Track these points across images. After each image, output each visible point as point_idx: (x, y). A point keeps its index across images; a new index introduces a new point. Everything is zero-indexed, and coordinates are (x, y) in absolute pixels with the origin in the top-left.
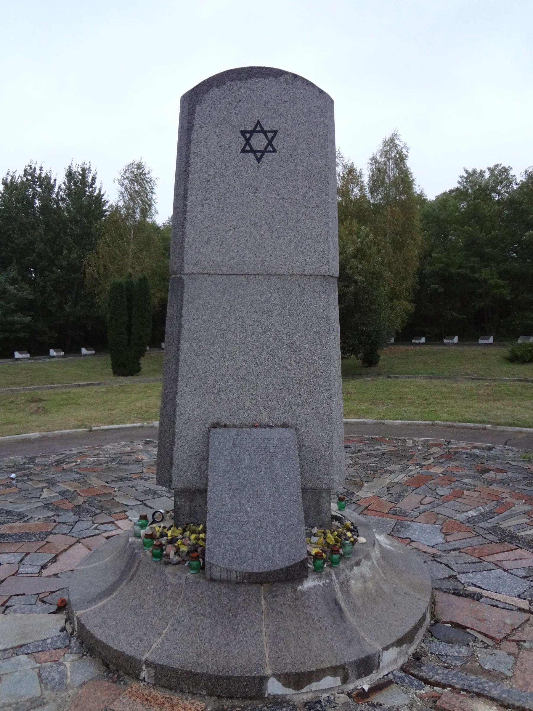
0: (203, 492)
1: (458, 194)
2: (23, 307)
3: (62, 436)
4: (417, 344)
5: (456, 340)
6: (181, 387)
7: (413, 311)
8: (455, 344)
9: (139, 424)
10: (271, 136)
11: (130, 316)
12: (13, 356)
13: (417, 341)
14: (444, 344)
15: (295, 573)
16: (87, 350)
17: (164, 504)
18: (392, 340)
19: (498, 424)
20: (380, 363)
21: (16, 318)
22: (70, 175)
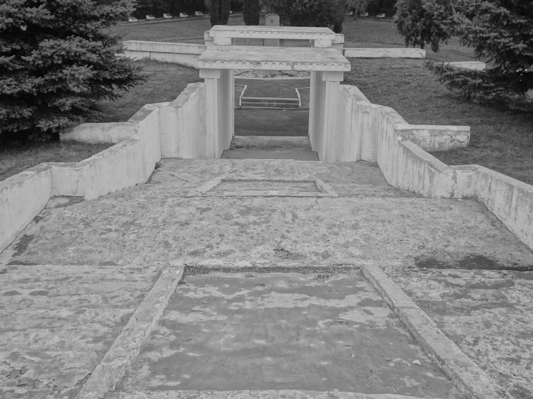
4: (379, 18)
13: (380, 16)
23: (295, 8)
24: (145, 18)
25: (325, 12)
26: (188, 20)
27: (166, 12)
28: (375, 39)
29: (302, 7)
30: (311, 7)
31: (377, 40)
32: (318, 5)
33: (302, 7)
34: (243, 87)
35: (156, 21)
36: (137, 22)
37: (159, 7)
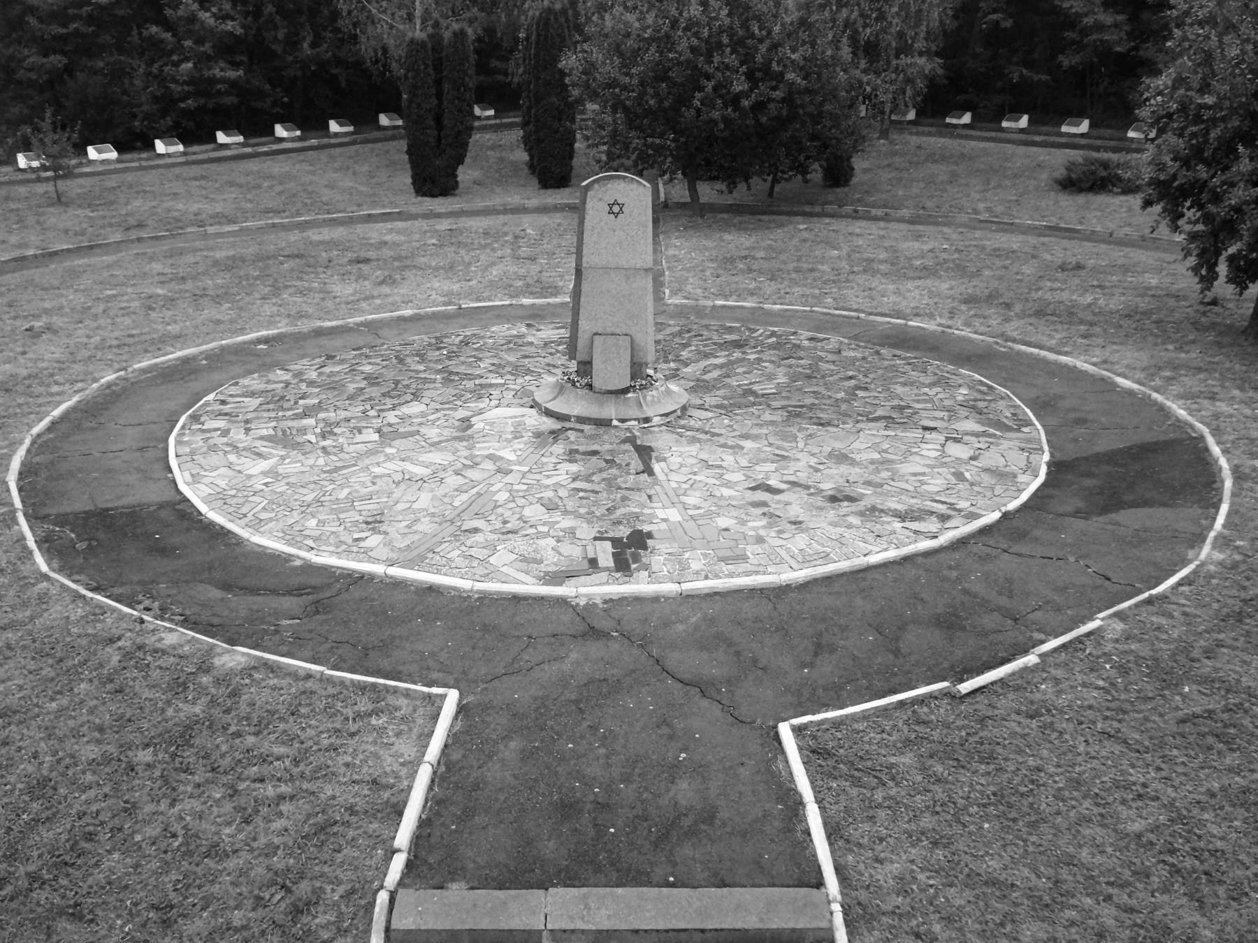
0: (590, 363)
2: (228, 48)
3: (434, 314)
4: (955, 126)
6: (581, 317)
9: (507, 303)
10: (621, 206)
11: (439, 95)
12: (272, 132)
13: (954, 121)
15: (625, 391)
16: (341, 125)
17: (573, 366)
18: (911, 115)
19: (871, 314)
20: (854, 180)
21: (217, 73)
23: (698, 111)
24: (214, 140)
25: (803, 124)
26: (353, 143)
27: (282, 121)
28: (976, 211)
29: (725, 106)
30: (759, 107)
31: (985, 216)
32: (783, 100)
33: (725, 106)
34: (435, 703)
35: (249, 150)
36: (184, 154)
37: (258, 105)
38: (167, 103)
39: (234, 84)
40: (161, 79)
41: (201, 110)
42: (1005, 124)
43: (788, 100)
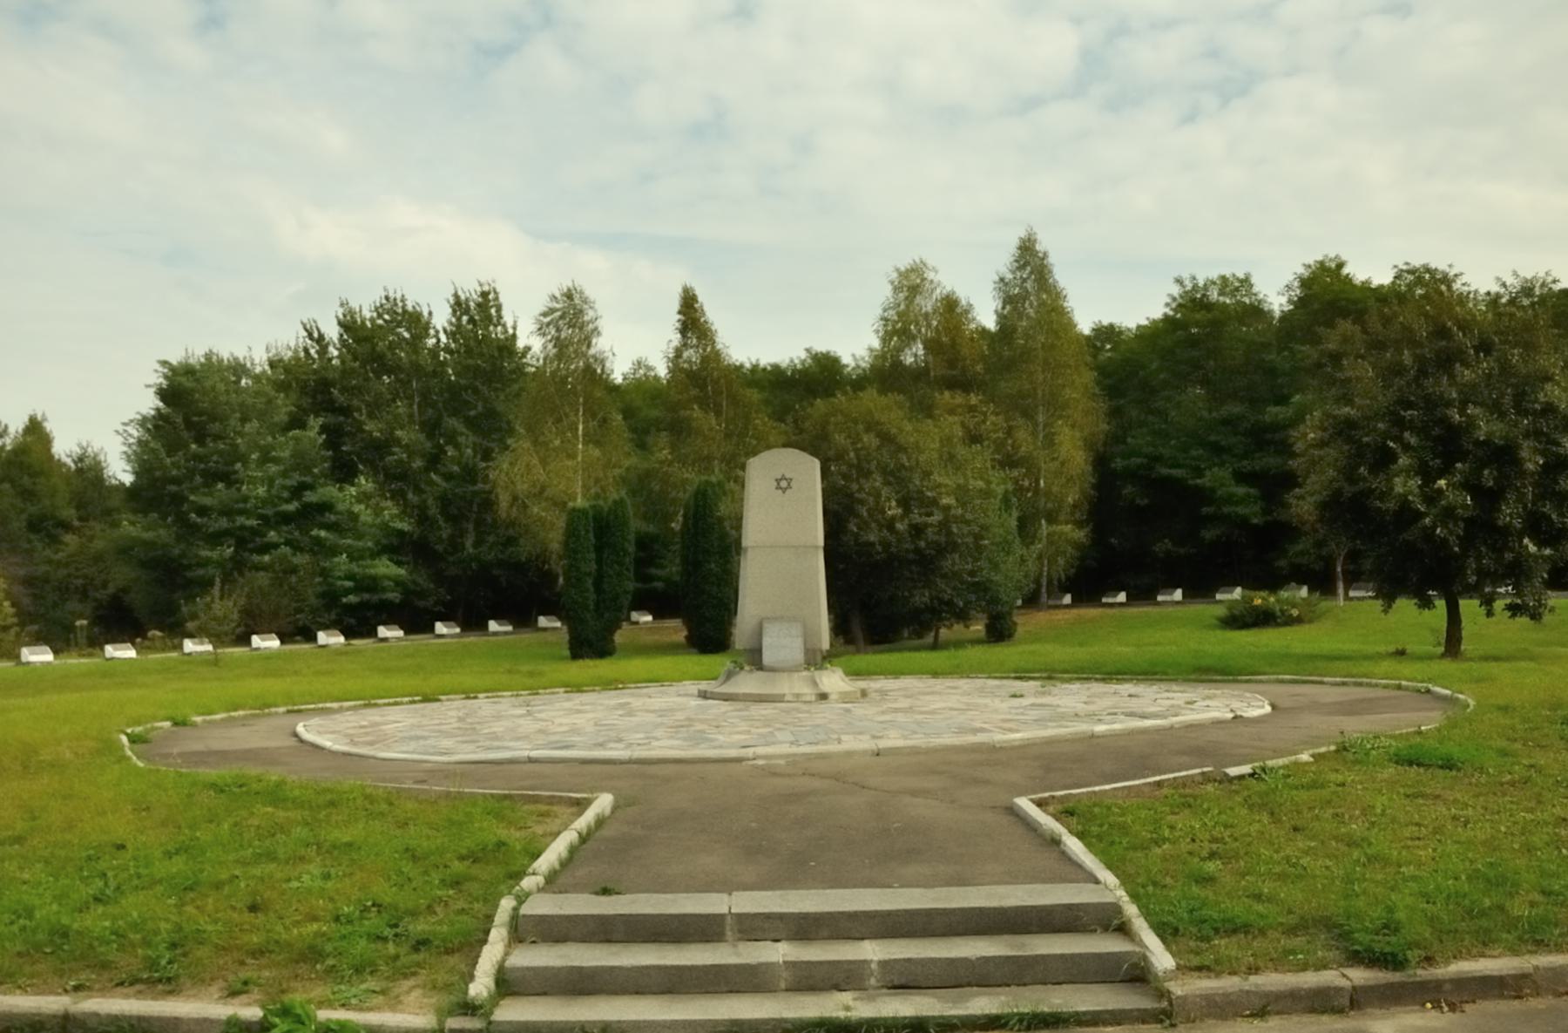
1: (1168, 325)
2: (395, 546)
4: (1112, 605)
5: (1178, 595)
7: (1500, 523)
8: (1178, 603)
12: (431, 629)
13: (1110, 600)
14: (1159, 604)
18: (1019, 602)
22: (459, 306)
37: (421, 604)
38: (331, 598)
39: (398, 583)
40: (324, 573)
41: (363, 605)
42: (1160, 598)
43: (944, 525)
